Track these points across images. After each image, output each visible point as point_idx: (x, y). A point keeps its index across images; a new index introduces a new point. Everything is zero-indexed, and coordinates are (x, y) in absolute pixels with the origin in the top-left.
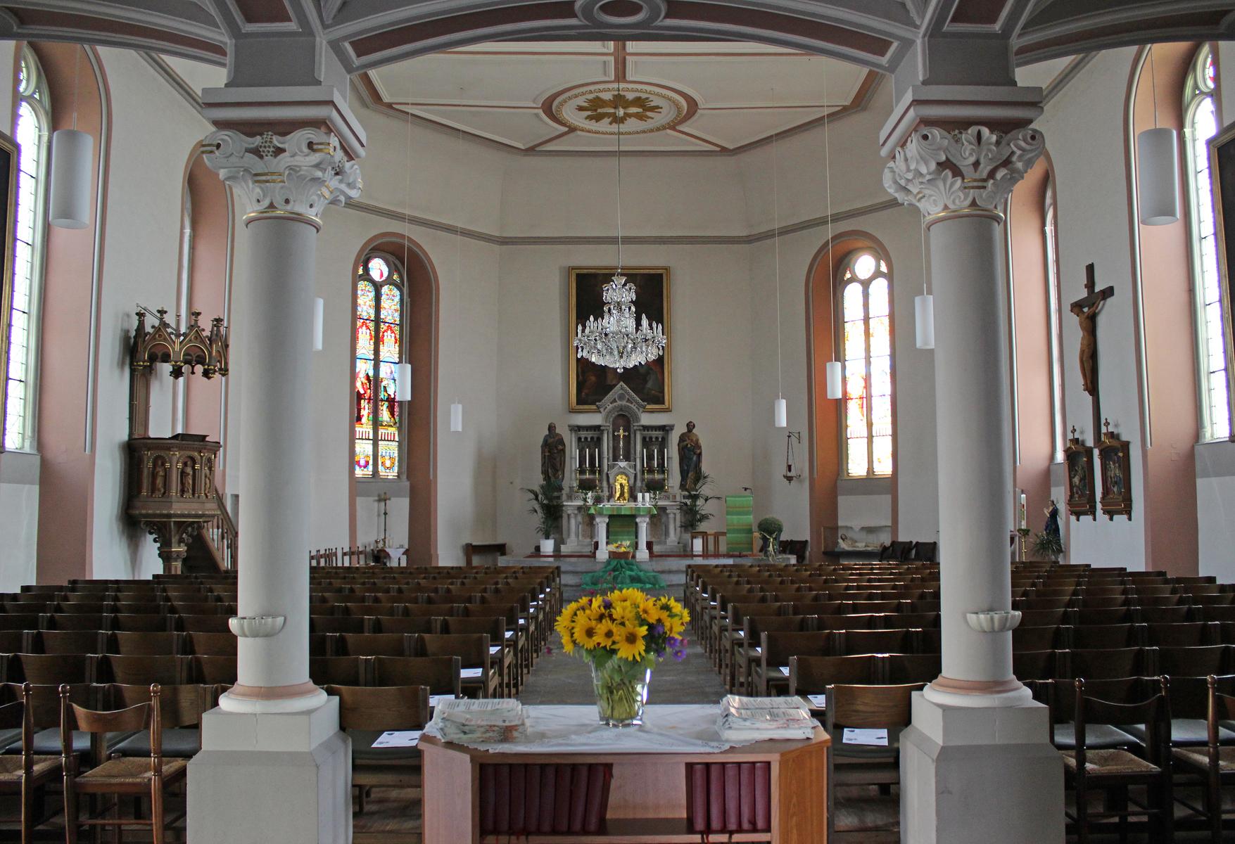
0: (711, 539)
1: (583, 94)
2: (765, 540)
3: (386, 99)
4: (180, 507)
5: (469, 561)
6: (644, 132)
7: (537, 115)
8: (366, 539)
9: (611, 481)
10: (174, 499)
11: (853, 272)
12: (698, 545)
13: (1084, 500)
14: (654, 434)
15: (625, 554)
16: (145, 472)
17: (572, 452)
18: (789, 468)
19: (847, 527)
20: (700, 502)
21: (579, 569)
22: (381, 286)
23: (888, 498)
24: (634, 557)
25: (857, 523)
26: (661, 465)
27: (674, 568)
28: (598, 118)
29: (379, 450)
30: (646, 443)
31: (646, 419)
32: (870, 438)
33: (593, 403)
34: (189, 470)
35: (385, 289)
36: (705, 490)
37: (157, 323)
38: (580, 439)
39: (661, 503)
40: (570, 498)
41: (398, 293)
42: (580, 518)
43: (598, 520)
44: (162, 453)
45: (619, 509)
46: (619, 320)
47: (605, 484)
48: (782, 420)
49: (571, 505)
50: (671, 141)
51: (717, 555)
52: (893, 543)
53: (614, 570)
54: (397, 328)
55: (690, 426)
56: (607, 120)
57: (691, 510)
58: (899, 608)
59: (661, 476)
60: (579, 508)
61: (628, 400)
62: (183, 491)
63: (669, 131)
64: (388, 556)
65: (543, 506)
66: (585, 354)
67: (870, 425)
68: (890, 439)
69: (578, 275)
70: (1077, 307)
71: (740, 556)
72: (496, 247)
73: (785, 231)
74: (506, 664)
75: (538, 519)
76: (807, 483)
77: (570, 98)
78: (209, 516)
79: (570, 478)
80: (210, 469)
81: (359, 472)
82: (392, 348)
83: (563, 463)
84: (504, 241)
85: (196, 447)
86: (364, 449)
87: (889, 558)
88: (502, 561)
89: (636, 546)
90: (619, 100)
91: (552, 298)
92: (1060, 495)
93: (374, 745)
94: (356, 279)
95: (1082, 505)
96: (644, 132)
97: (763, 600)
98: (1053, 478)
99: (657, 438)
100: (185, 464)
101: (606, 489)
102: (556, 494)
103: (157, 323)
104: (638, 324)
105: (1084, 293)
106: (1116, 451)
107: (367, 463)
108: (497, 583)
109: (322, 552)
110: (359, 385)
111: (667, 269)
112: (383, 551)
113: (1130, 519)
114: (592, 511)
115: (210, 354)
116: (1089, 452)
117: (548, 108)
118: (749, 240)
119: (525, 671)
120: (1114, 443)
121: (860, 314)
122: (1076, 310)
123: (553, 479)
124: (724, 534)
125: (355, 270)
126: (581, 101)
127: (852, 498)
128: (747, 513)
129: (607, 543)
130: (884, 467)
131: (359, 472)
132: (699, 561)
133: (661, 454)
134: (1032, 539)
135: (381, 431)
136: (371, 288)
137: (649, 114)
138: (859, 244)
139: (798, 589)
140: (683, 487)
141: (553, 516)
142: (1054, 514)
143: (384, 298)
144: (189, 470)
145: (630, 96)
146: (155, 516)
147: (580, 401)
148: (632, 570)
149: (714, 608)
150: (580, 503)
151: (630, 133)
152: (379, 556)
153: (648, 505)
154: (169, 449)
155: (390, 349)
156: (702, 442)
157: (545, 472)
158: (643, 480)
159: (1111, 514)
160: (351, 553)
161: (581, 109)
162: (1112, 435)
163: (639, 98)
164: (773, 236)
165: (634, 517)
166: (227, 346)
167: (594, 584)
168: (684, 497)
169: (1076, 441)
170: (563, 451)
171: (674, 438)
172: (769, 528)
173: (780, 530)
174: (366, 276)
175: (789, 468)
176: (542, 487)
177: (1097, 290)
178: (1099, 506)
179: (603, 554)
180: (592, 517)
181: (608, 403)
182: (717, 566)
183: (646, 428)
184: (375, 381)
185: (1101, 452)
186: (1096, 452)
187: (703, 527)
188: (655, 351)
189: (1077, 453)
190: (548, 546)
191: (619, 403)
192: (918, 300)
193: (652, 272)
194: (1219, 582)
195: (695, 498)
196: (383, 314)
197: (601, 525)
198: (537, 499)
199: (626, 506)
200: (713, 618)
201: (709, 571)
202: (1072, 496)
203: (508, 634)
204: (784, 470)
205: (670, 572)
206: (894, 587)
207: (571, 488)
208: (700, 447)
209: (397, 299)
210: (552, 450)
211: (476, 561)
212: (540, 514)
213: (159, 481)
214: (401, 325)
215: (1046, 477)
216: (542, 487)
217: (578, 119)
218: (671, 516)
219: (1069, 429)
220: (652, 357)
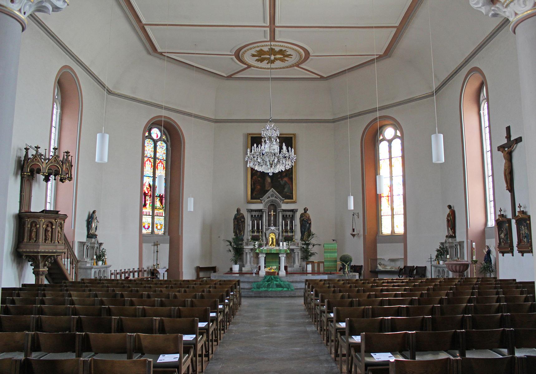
0: (316, 265)
1: (254, 48)
2: (344, 266)
3: (159, 50)
4: (44, 248)
5: (198, 275)
6: (284, 68)
7: (232, 59)
8: (148, 264)
9: (267, 236)
10: (41, 243)
11: (383, 136)
12: (309, 268)
13: (507, 246)
14: (288, 213)
15: (273, 273)
16: (26, 229)
17: (248, 222)
18: (354, 230)
19: (381, 259)
21: (250, 280)
22: (157, 142)
23: (403, 244)
24: (278, 274)
25: (387, 257)
26: (291, 228)
27: (298, 280)
28: (261, 60)
29: (155, 221)
30: (284, 218)
31: (284, 207)
32: (393, 215)
33: (259, 199)
34: (49, 229)
35: (159, 143)
36: (313, 241)
37: (34, 153)
38: (252, 216)
39: (291, 247)
40: (247, 244)
41: (165, 145)
42: (252, 254)
43: (260, 255)
44: (35, 220)
45: (271, 250)
46: (270, 147)
47: (264, 238)
48: (351, 207)
49: (247, 248)
50: (297, 73)
51: (319, 273)
52: (405, 267)
53: (268, 281)
54: (164, 162)
55: (306, 210)
56: (266, 62)
57: (306, 250)
58: (411, 302)
60: (252, 250)
61: (276, 197)
62: (46, 240)
63: (295, 68)
64: (158, 272)
65: (234, 248)
66: (251, 165)
67: (392, 209)
68: (403, 216)
69: (252, 137)
70: (501, 148)
71: (331, 274)
73: (352, 116)
74: (210, 333)
75: (232, 254)
76: (362, 238)
77: (248, 50)
78: (60, 252)
79: (247, 235)
80: (61, 228)
81: (144, 231)
82: (162, 171)
84: (217, 121)
85: (54, 217)
86: (147, 220)
87: (403, 274)
88: (214, 276)
89: (279, 269)
90: (272, 51)
91: (237, 137)
92: (492, 243)
93: (158, 361)
94: (144, 138)
95: (505, 247)
96: (284, 68)
97: (351, 304)
98: (377, 241)
99: (289, 216)
100: (47, 226)
101: (264, 240)
102: (240, 243)
103: (34, 153)
104: (281, 148)
105: (505, 141)
106: (524, 220)
107: (149, 227)
108: (203, 291)
109: (123, 271)
110: (145, 189)
111: (294, 135)
112: (155, 270)
113: (513, 255)
114: (257, 251)
115: (62, 169)
116: (509, 221)
117: (237, 55)
118: (334, 121)
119: (228, 323)
120: (524, 216)
121: (387, 156)
122: (501, 149)
124: (323, 262)
125: (144, 134)
126: (253, 52)
127: (383, 245)
128: (334, 252)
129: (265, 267)
130: (400, 230)
131: (144, 231)
132: (310, 277)
134: (478, 265)
135: (156, 211)
136: (152, 143)
137: (286, 58)
138: (386, 123)
139: (369, 296)
140: (302, 239)
141: (239, 253)
142: (489, 252)
143: (158, 147)
144: (49, 229)
145: (277, 49)
146: (30, 252)
147: (252, 199)
148: (277, 281)
149: (312, 295)
150: (252, 247)
151: (277, 69)
152: (154, 273)
153: (285, 248)
154: (39, 218)
155: (161, 172)
156: (311, 217)
157: (235, 232)
158: (283, 236)
159: (522, 253)
160: (139, 271)
161: (253, 56)
162: (523, 212)
163: (281, 50)
164: (347, 118)
165: (278, 254)
166: (72, 166)
167: (258, 288)
168: (303, 244)
169: (502, 216)
170: (244, 221)
171: (298, 215)
172: (345, 260)
173: (351, 261)
174: (150, 137)
175: (354, 230)
176: (233, 239)
177: (512, 139)
178: (515, 249)
179: (263, 273)
180: (258, 254)
181: (266, 198)
182: (321, 280)
184: (153, 187)
185: (516, 222)
186: (513, 222)
187: (312, 259)
188: (290, 163)
189: (502, 222)
190: (236, 268)
191: (271, 198)
192: (433, 137)
193: (288, 136)
194: (517, 281)
195: (308, 245)
196: (158, 155)
197: (262, 258)
198: (231, 245)
199: (274, 249)
200: (312, 299)
201: (317, 284)
202: (500, 243)
203: (220, 307)
204: (351, 231)
205: (296, 282)
206: (405, 290)
207: (248, 240)
208: (310, 220)
209: (165, 148)
210: (239, 221)
211: (201, 275)
212: (233, 252)
213: (33, 234)
214: (167, 160)
215: (484, 234)
216: (233, 239)
217: (252, 61)
218: (296, 253)
219: (498, 209)
220: (288, 167)
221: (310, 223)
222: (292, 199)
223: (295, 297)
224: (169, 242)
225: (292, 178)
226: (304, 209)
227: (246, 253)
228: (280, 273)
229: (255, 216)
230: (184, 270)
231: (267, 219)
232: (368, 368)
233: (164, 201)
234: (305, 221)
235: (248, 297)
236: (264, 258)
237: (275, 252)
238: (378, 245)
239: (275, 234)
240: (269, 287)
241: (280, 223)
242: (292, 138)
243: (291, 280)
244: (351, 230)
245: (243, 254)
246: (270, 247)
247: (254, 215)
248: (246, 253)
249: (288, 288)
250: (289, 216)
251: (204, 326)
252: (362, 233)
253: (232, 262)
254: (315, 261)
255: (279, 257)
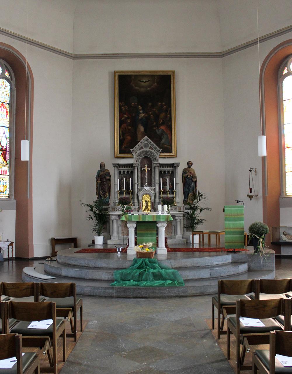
9: (140, 199)
14: (167, 169)
15: (148, 255)
17: (116, 181)
18: (251, 190)
20: (197, 212)
24: (156, 253)
26: (172, 188)
31: (161, 161)
36: (201, 204)
38: (120, 173)
40: (114, 210)
41: (8, 84)
45: (144, 217)
47: (136, 201)
49: (114, 214)
53: (139, 268)
54: (8, 107)
55: (190, 164)
59: (171, 196)
65: (95, 214)
69: (120, 76)
72: (70, 60)
75: (93, 222)
76: (261, 200)
79: (114, 197)
83: (109, 187)
101: (136, 204)
102: (104, 207)
111: (173, 72)
118: (222, 55)
123: (103, 198)
124: (217, 234)
133: (171, 181)
140: (185, 202)
141: (103, 222)
147: (121, 152)
148: (154, 268)
153: (166, 214)
156: (197, 174)
157: (98, 193)
158: (160, 198)
165: (155, 222)
168: (186, 209)
175: (251, 190)
176: (96, 202)
179: (133, 250)
181: (137, 151)
183: (162, 165)
187: (199, 228)
190: (99, 241)
191: (145, 149)
195: (194, 209)
198: (92, 210)
199: (150, 215)
205: (185, 268)
207: (115, 203)
208: (196, 177)
209: (8, 87)
210: (103, 180)
221: (196, 181)
222: (171, 152)
223: (186, 296)
224: (15, 209)
225: (171, 125)
226: (188, 163)
227: (113, 220)
228: (159, 252)
229: (124, 172)
230: (284, 184)
231: (140, 176)
232: (223, 306)
233: (8, 156)
234: (189, 179)
235: (106, 297)
236: (134, 229)
237: (151, 220)
238: (282, 210)
239: (150, 195)
240: (142, 282)
241: (157, 182)
242: (170, 76)
243: (177, 266)
244: (248, 190)
245: (109, 222)
246: (144, 213)
247: (122, 171)
248: (113, 220)
249: (173, 280)
250: (169, 172)
251: (46, 327)
252: (261, 194)
253: (95, 232)
254: (204, 231)
255: (157, 227)
